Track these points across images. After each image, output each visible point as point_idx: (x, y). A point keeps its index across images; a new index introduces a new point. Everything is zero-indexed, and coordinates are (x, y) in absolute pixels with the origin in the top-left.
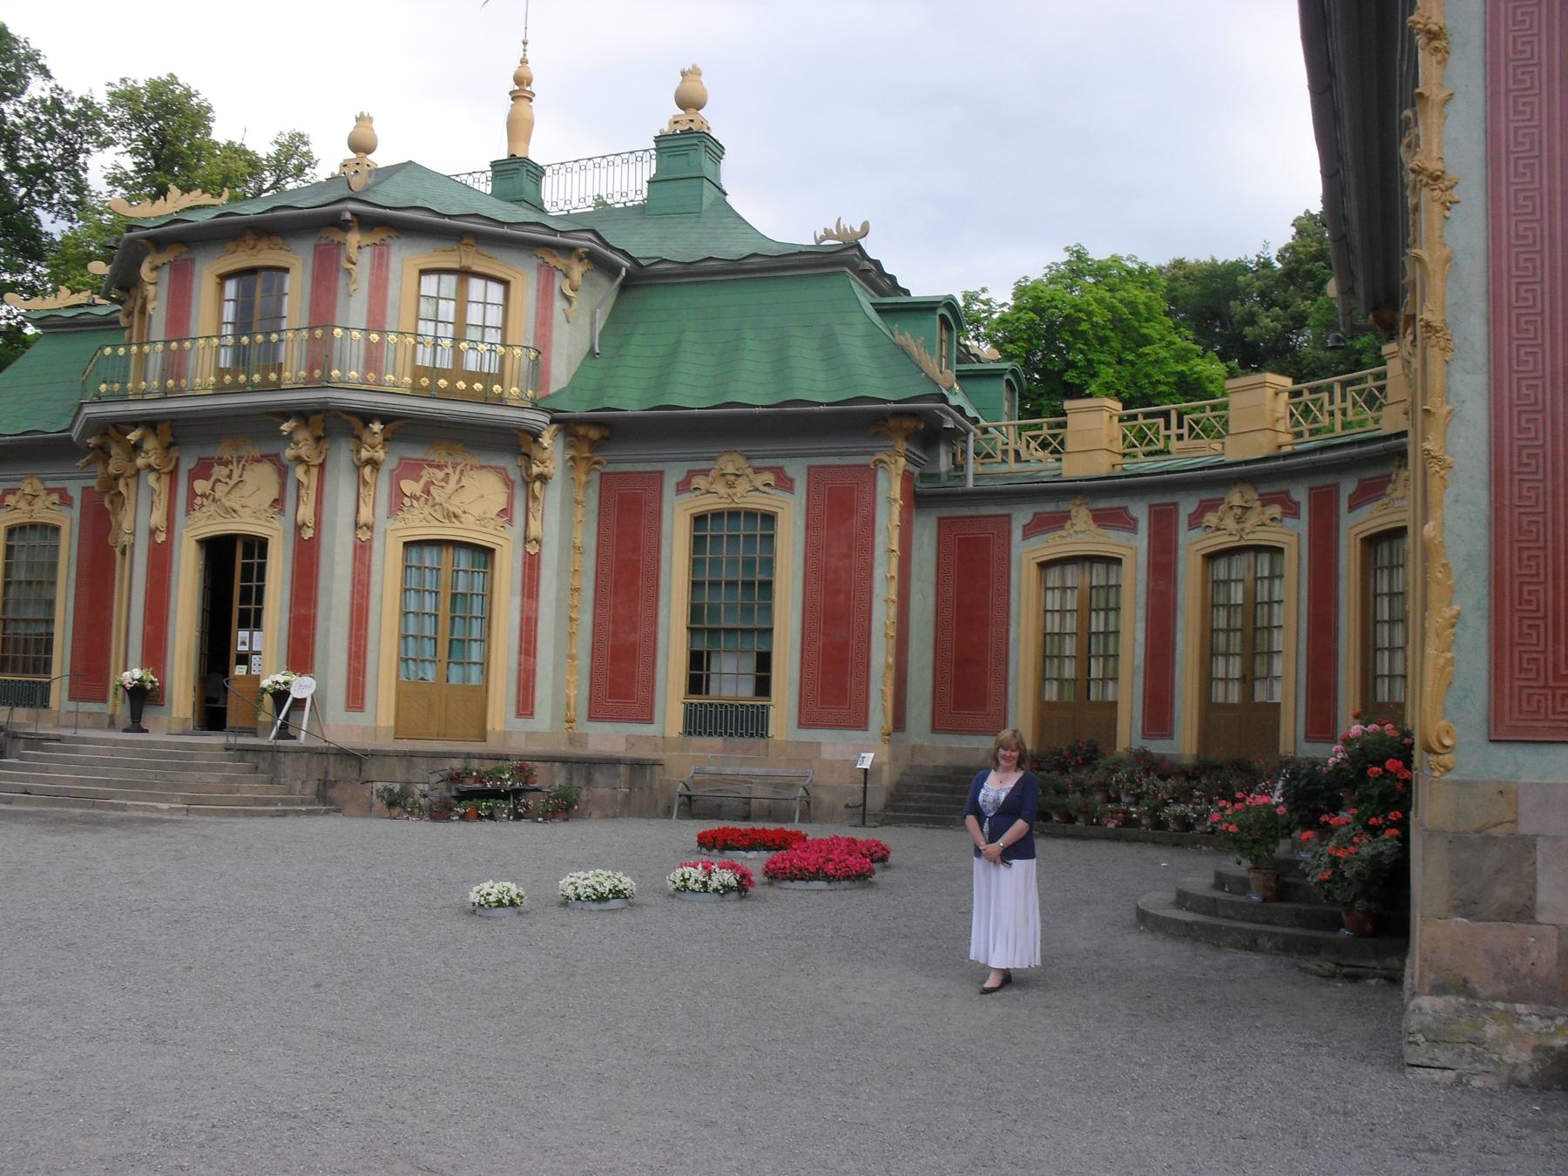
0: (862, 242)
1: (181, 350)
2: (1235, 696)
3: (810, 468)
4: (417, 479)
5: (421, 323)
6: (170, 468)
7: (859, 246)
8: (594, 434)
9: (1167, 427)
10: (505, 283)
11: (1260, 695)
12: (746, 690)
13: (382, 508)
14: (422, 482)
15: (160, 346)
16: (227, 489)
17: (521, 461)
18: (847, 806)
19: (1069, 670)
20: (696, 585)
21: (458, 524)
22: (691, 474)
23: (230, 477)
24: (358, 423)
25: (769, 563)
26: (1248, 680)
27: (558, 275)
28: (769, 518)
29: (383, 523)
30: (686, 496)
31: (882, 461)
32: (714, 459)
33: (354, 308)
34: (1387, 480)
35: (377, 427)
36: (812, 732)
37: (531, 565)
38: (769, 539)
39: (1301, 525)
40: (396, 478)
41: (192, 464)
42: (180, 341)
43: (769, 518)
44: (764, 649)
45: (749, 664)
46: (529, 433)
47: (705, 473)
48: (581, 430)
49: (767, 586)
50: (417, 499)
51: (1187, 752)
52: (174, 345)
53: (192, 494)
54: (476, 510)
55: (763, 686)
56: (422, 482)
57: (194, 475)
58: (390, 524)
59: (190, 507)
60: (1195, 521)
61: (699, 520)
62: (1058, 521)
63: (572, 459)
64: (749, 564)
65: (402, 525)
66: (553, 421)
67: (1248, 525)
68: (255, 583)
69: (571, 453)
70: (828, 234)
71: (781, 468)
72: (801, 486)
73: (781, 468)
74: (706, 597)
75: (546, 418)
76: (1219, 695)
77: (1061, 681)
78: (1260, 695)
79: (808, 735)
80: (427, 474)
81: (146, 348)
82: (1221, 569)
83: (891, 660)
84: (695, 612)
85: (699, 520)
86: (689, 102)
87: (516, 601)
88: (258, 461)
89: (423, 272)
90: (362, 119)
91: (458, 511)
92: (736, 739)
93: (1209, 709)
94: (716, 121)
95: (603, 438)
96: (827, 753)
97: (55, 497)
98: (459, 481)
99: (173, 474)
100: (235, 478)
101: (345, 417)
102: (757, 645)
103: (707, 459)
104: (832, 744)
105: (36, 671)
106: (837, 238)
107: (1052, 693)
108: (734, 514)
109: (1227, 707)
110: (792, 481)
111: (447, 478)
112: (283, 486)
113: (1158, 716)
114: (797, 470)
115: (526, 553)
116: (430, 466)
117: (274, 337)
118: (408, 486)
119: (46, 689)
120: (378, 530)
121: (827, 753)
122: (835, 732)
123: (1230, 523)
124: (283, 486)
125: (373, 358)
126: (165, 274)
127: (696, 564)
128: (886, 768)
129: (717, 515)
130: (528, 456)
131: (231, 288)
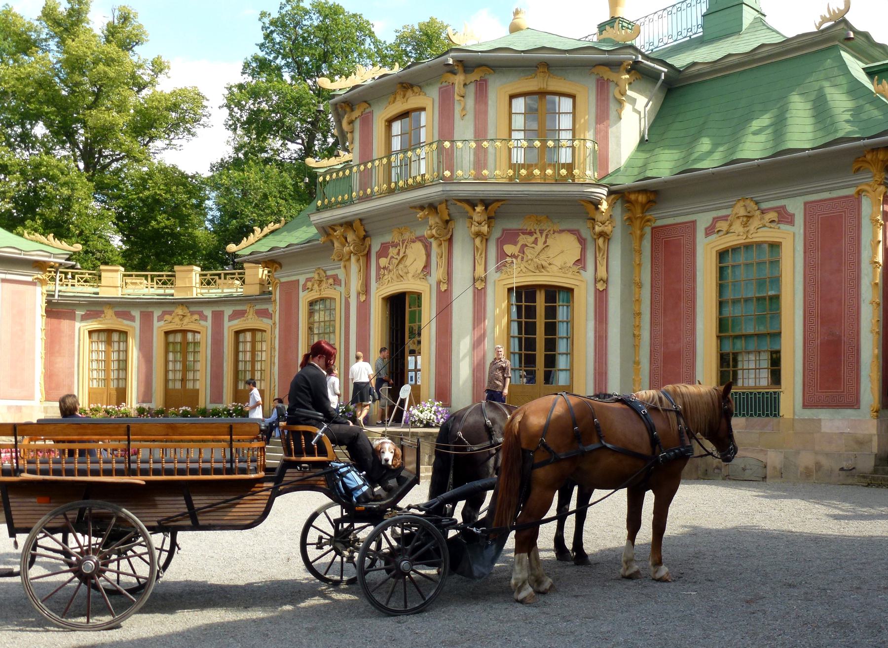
0: (847, 17)
2: (178, 385)
3: (806, 204)
4: (515, 243)
5: (513, 133)
6: (449, 236)
7: (845, 21)
8: (642, 198)
10: (573, 97)
11: (190, 385)
12: (764, 380)
13: (492, 267)
14: (519, 245)
16: (397, 262)
17: (589, 224)
18: (842, 469)
20: (721, 304)
21: (545, 273)
22: (716, 220)
23: (398, 254)
24: (468, 208)
25: (776, 281)
26: (184, 380)
27: (612, 85)
28: (775, 246)
29: (493, 275)
30: (714, 237)
31: (863, 191)
32: (732, 206)
33: (464, 128)
34: (103, 312)
35: (479, 209)
36: (815, 411)
37: (601, 298)
38: (775, 263)
39: (137, 324)
40: (501, 242)
43: (775, 246)
44: (776, 348)
45: (765, 363)
46: (592, 202)
47: (725, 218)
48: (633, 197)
49: (775, 299)
50: (516, 257)
52: (362, 167)
53: (379, 268)
54: (558, 262)
55: (776, 376)
56: (519, 245)
57: (380, 255)
58: (497, 276)
59: (378, 278)
60: (160, 319)
61: (722, 255)
63: (629, 219)
64: (761, 283)
65: (505, 276)
66: (610, 193)
67: (752, 228)
69: (629, 214)
70: (824, 20)
71: (784, 207)
72: (799, 220)
73: (784, 207)
74: (728, 311)
75: (604, 191)
78: (190, 385)
79: (809, 413)
80: (523, 239)
82: (171, 338)
83: (876, 351)
84: (722, 324)
87: (591, 325)
88: (414, 242)
89: (512, 97)
91: (544, 263)
92: (756, 419)
93: (167, 392)
95: (649, 202)
98: (545, 242)
99: (368, 256)
100: (401, 255)
101: (459, 204)
102: (767, 345)
103: (727, 208)
104: (833, 422)
106: (830, 20)
108: (748, 247)
109: (174, 390)
111: (535, 242)
112: (428, 256)
113: (217, 396)
114: (796, 207)
115: (596, 290)
116: (524, 233)
117: (369, 165)
118: (509, 249)
120: (490, 281)
122: (831, 411)
123: (177, 320)
124: (428, 256)
125: (480, 160)
126: (472, 88)
127: (721, 288)
128: (875, 439)
129: (735, 249)
130: (594, 219)
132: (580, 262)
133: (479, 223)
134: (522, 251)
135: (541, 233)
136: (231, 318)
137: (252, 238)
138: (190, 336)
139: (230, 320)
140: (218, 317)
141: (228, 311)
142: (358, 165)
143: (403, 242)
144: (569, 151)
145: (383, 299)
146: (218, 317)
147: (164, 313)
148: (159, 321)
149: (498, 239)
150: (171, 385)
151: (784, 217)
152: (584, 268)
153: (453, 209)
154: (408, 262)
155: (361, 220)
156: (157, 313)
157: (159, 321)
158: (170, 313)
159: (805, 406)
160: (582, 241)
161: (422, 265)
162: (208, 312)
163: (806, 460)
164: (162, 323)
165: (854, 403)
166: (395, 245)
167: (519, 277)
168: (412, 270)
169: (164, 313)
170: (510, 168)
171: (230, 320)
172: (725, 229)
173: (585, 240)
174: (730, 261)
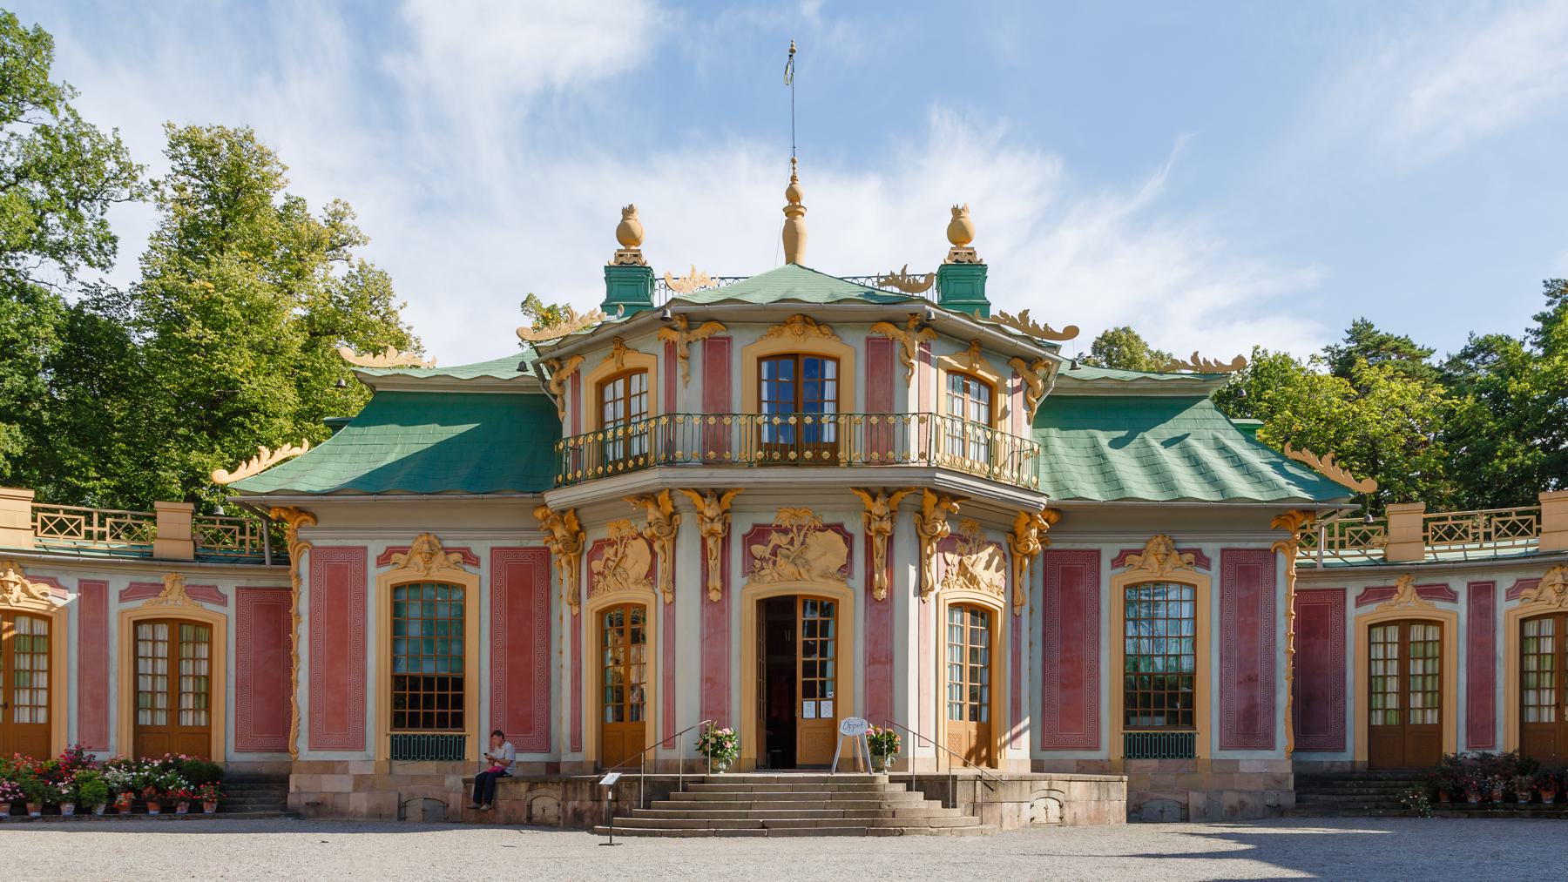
1: (719, 424)
2: (162, 719)
9: (89, 523)
15: (697, 420)
19: (1393, 702)
41: (747, 529)
42: (720, 416)
51: (1359, 759)
52: (600, 436)
53: (591, 573)
60: (1511, 594)
61: (396, 589)
62: (1386, 593)
68: (818, 639)
76: (1532, 716)
77: (1385, 710)
81: (727, 421)
82: (1378, 635)
85: (396, 589)
86: (626, 234)
90: (628, 212)
92: (1169, 761)
93: (139, 731)
94: (984, 248)
96: (1244, 768)
97: (1189, 557)
104: (1251, 761)
105: (443, 723)
107: (1378, 719)
109: (1539, 724)
110: (478, 559)
112: (654, 554)
118: (757, 549)
119: (460, 743)
121: (1244, 768)
129: (416, 585)
131: (765, 365)
132: (846, 569)
133: (712, 520)
134: (774, 553)
135: (799, 530)
136: (1360, 601)
137: (255, 466)
138: (1417, 633)
139: (1358, 605)
140: (1482, 594)
141: (1505, 582)
142: (596, 433)
143: (800, 528)
144: (832, 427)
145: (759, 602)
146: (1482, 594)
147: (1521, 584)
148: (1508, 598)
149: (744, 536)
150: (1532, 716)
151: (1201, 560)
152: (850, 575)
153: (679, 501)
154: (628, 564)
155: (576, 510)
156: (1505, 582)
157: (1508, 598)
158: (1535, 583)
159: (1221, 748)
160: (848, 539)
161: (646, 569)
162: (1460, 585)
163: (1230, 799)
164: (1516, 603)
165: (1270, 746)
166: (611, 543)
167: (773, 585)
168: (633, 574)
169: (1521, 584)
170: (759, 448)
171: (1358, 605)
172: (403, 563)
173: (851, 536)
174: (404, 594)
